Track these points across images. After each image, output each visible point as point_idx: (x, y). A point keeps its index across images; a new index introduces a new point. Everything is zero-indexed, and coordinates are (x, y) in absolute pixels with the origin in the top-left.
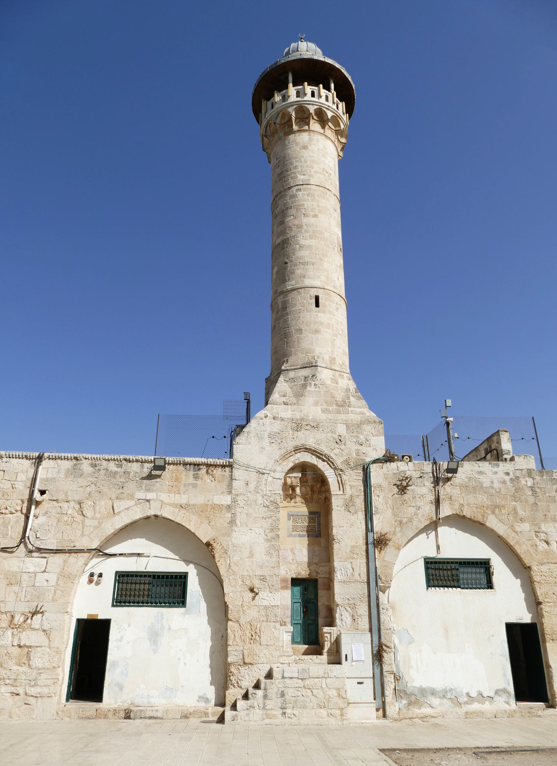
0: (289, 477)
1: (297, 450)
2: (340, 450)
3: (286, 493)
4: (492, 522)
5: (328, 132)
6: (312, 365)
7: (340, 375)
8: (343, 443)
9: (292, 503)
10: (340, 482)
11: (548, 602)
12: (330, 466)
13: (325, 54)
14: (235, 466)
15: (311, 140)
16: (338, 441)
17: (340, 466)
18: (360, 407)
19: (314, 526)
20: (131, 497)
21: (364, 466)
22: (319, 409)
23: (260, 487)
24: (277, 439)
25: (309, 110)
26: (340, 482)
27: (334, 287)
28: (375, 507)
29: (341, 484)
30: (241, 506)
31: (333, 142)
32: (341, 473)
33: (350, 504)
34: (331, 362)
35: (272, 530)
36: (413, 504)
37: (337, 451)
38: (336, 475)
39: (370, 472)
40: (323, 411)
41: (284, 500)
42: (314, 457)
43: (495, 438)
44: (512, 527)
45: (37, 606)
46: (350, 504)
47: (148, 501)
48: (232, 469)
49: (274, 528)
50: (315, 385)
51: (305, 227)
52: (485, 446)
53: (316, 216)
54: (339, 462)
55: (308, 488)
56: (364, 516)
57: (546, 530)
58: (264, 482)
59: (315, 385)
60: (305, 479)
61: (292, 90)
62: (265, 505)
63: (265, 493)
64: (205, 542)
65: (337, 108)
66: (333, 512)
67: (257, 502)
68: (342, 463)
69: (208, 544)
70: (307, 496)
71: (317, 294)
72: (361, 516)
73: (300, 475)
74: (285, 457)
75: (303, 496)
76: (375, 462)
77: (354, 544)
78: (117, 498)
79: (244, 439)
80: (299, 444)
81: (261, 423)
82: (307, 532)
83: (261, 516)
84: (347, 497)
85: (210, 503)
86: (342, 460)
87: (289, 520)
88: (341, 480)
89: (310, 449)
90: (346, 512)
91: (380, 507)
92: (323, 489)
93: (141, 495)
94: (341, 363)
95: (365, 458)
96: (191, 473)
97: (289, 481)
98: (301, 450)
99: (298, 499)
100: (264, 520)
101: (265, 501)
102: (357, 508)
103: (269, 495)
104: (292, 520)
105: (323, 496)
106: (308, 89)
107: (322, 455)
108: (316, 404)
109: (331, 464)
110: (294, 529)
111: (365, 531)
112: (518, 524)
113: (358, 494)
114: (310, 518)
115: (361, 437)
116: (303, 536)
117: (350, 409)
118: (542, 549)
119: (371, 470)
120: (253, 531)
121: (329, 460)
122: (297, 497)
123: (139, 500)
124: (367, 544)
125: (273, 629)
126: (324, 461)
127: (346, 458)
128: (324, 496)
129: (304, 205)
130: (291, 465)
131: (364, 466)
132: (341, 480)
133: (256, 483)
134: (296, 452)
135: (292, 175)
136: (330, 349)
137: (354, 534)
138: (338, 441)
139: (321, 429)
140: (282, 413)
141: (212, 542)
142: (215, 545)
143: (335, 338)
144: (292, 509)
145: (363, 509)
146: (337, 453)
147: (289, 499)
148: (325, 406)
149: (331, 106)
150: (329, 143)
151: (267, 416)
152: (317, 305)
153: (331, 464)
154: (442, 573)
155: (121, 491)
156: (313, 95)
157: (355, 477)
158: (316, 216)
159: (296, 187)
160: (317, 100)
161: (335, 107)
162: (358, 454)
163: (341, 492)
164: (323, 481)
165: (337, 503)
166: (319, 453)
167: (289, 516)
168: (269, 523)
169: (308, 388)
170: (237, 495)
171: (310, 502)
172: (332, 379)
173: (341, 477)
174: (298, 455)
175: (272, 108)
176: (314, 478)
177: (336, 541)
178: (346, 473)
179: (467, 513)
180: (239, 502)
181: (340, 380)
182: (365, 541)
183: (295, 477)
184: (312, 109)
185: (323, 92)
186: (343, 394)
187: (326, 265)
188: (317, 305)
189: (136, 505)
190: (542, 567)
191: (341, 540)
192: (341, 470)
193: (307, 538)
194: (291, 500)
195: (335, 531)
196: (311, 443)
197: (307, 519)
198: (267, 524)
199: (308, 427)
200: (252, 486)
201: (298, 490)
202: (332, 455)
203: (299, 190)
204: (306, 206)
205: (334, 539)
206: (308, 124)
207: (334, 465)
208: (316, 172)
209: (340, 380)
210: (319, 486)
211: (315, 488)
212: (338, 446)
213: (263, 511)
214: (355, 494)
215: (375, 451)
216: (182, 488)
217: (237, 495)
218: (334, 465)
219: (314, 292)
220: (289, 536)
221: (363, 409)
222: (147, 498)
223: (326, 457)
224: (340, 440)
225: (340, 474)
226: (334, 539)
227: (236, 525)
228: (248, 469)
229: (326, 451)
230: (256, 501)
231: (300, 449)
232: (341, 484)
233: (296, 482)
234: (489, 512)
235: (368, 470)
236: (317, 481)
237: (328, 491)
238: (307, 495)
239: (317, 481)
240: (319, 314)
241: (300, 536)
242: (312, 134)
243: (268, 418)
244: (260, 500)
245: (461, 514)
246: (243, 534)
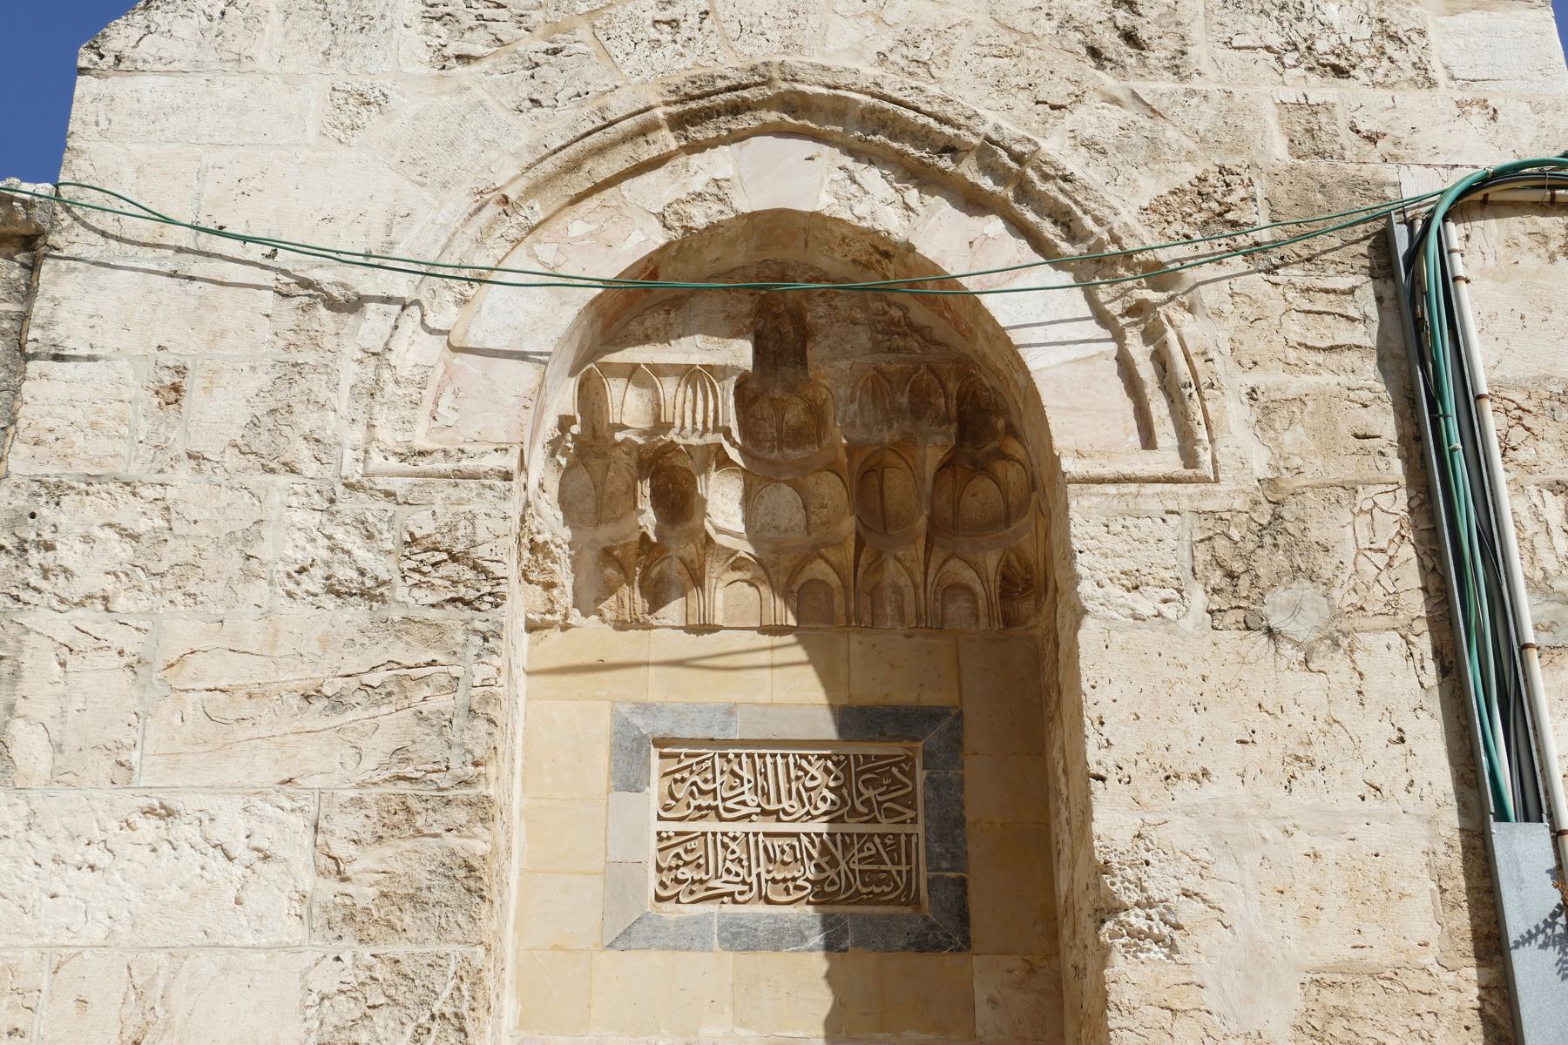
0: (632, 373)
2: (1130, 114)
3: (605, 534)
8: (1158, 55)
9: (667, 633)
10: (1146, 371)
12: (1038, 243)
13: (995, 183)
14: (69, 238)
16: (1110, 42)
17: (1142, 236)
19: (896, 847)
21: (1383, 242)
23: (308, 420)
24: (507, 30)
26: (1146, 371)
29: (1163, 392)
30: (77, 590)
33: (1268, 563)
35: (399, 819)
37: (1092, 118)
38: (1102, 317)
39: (1448, 282)
41: (588, 603)
42: (872, 176)
46: (1268, 563)
48: (32, 268)
49: (433, 795)
54: (1125, 204)
55: (831, 490)
56: (1431, 676)
58: (349, 373)
60: (794, 414)
62: (345, 573)
63: (353, 472)
66: (1089, 636)
67: (264, 551)
68: (1157, 210)
70: (819, 570)
72: (1397, 675)
73: (741, 353)
74: (588, 166)
75: (780, 567)
76: (1480, 197)
77: (1333, 947)
79: (183, 28)
80: (727, 61)
82: (822, 896)
83: (296, 677)
84: (1228, 495)
86: (1151, 187)
87: (631, 783)
88: (1161, 361)
89: (837, 109)
90: (1230, 638)
92: (982, 495)
95: (1389, 173)
97: (628, 408)
98: (746, 121)
99: (727, 596)
100: (315, 717)
101: (352, 541)
102: (1342, 597)
103: (398, 485)
104: (656, 788)
105: (979, 570)
107: (951, 149)
109: (1049, 230)
110: (683, 871)
111: (1451, 819)
113: (1348, 469)
114: (854, 777)
116: (780, 939)
119: (1459, 267)
120: (184, 830)
121: (1025, 192)
122: (716, 575)
124: (1491, 944)
126: (973, 202)
127: (1190, 172)
128: (992, 561)
131: (1383, 242)
132: (1161, 361)
133: (263, 380)
134: (696, 133)
137: (1332, 849)
138: (1110, 42)
144: (657, 687)
145: (1416, 604)
146: (1106, 137)
147: (633, 598)
153: (1049, 230)
157: (1295, 328)
162: (1309, 135)
163: (1166, 458)
164: (971, 410)
165: (1121, 551)
166: (921, 137)
167: (634, 749)
168: (379, 747)
170: (55, 491)
171: (853, 621)
173: (1153, 335)
174: (721, 162)
176: (878, 386)
177: (1136, 920)
178: (1209, 297)
180: (69, 553)
182: (1462, 920)
183: (689, 374)
191: (1188, 911)
192: (1159, 276)
193: (819, 963)
194: (657, 597)
195: (1112, 821)
197: (819, 776)
198: (344, 758)
200: (218, 412)
201: (722, 504)
202: (1055, 147)
205: (1108, 909)
207: (1073, 232)
210: (932, 455)
211: (897, 485)
212: (1108, 80)
213: (325, 639)
214: (1317, 468)
215: (1478, 118)
217: (55, 491)
218: (1073, 232)
220: (624, 940)
223: (988, 168)
224: (1130, 38)
225: (1138, 310)
226: (1108, 909)
228: (199, 267)
229: (999, 116)
231: (735, 109)
232: (1163, 392)
233: (701, 416)
235: (1430, 267)
236: (919, 407)
237: (1038, 493)
238: (815, 552)
239: (919, 407)
241: (739, 939)
244: (293, 531)
246: (77, 852)
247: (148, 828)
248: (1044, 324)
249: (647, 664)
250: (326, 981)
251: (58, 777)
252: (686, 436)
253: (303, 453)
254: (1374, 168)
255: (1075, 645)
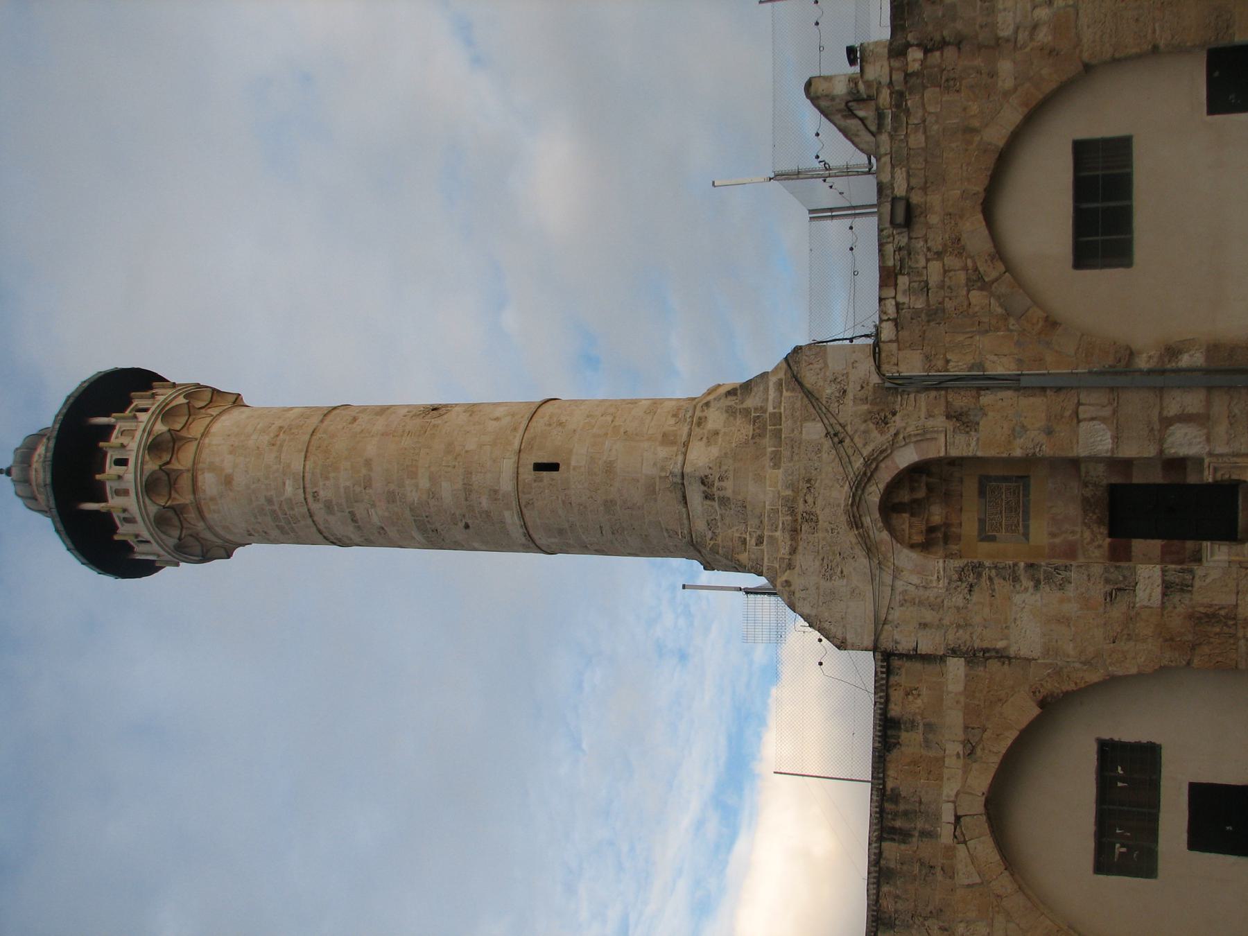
1: (855, 522)
4: (996, 135)
5: (197, 429)
6: (680, 485)
7: (699, 424)
11: (1154, 32)
15: (213, 468)
18: (766, 390)
20: (949, 852)
22: (770, 472)
23: (932, 599)
24: (834, 564)
25: (154, 473)
27: (515, 429)
28: (971, 369)
31: (215, 418)
32: (901, 436)
34: (673, 443)
35: (1016, 579)
36: (964, 292)
40: (776, 466)
43: (823, 103)
44: (1006, 94)
45: (748, 592)
47: (958, 818)
48: (895, 655)
50: (721, 479)
51: (392, 487)
52: (838, 117)
53: (368, 463)
57: (1012, 27)
59: (721, 479)
61: (114, 502)
64: (1036, 711)
65: (146, 410)
68: (882, 432)
69: (1043, 704)
71: (531, 467)
76: (878, 367)
78: (952, 877)
81: (803, 594)
85: (962, 699)
86: (875, 434)
91: (969, 359)
93: (946, 833)
94: (672, 421)
95: (871, 385)
96: (904, 736)
106: (111, 470)
108: (760, 479)
112: (1000, 83)
115: (828, 391)
117: (770, 409)
118: (1050, 38)
123: (955, 837)
125: (1208, 581)
129: (346, 488)
130: (885, 535)
135: (285, 507)
136: (646, 445)
139: (814, 473)
140: (782, 551)
141: (1039, 696)
142: (1044, 692)
143: (622, 430)
148: (767, 462)
149: (142, 426)
150: (217, 427)
151: (786, 581)
152: (554, 467)
154: (1103, 226)
155: (938, 869)
156: (122, 462)
158: (368, 463)
159: (310, 499)
160: (134, 454)
161: (144, 417)
167: (985, 537)
169: (728, 493)
172: (709, 443)
175: (148, 542)
179: (979, 188)
181: (710, 426)
183: (910, 526)
184: (152, 466)
185: (115, 439)
186: (738, 422)
187: (471, 445)
188: (554, 467)
189: (965, 842)
190: (1085, 40)
196: (840, 494)
198: (1002, 586)
199: (810, 500)
203: (315, 495)
204: (348, 484)
206: (180, 472)
208: (278, 458)
209: (710, 426)
216: (932, 754)
218: (885, 450)
219: (528, 474)
221: (771, 384)
222: (952, 819)
226: (1034, 454)
227: (1005, 649)
230: (958, 608)
234: (977, 138)
240: (573, 463)
242: (201, 465)
243: (790, 579)
245: (982, 195)
247: (1018, 622)
248: (907, 457)
249: (525, 526)
250: (1048, 589)
251: (1007, 638)
252: (924, 528)
253: (939, 600)
254: (870, 387)
255: (55, 422)
